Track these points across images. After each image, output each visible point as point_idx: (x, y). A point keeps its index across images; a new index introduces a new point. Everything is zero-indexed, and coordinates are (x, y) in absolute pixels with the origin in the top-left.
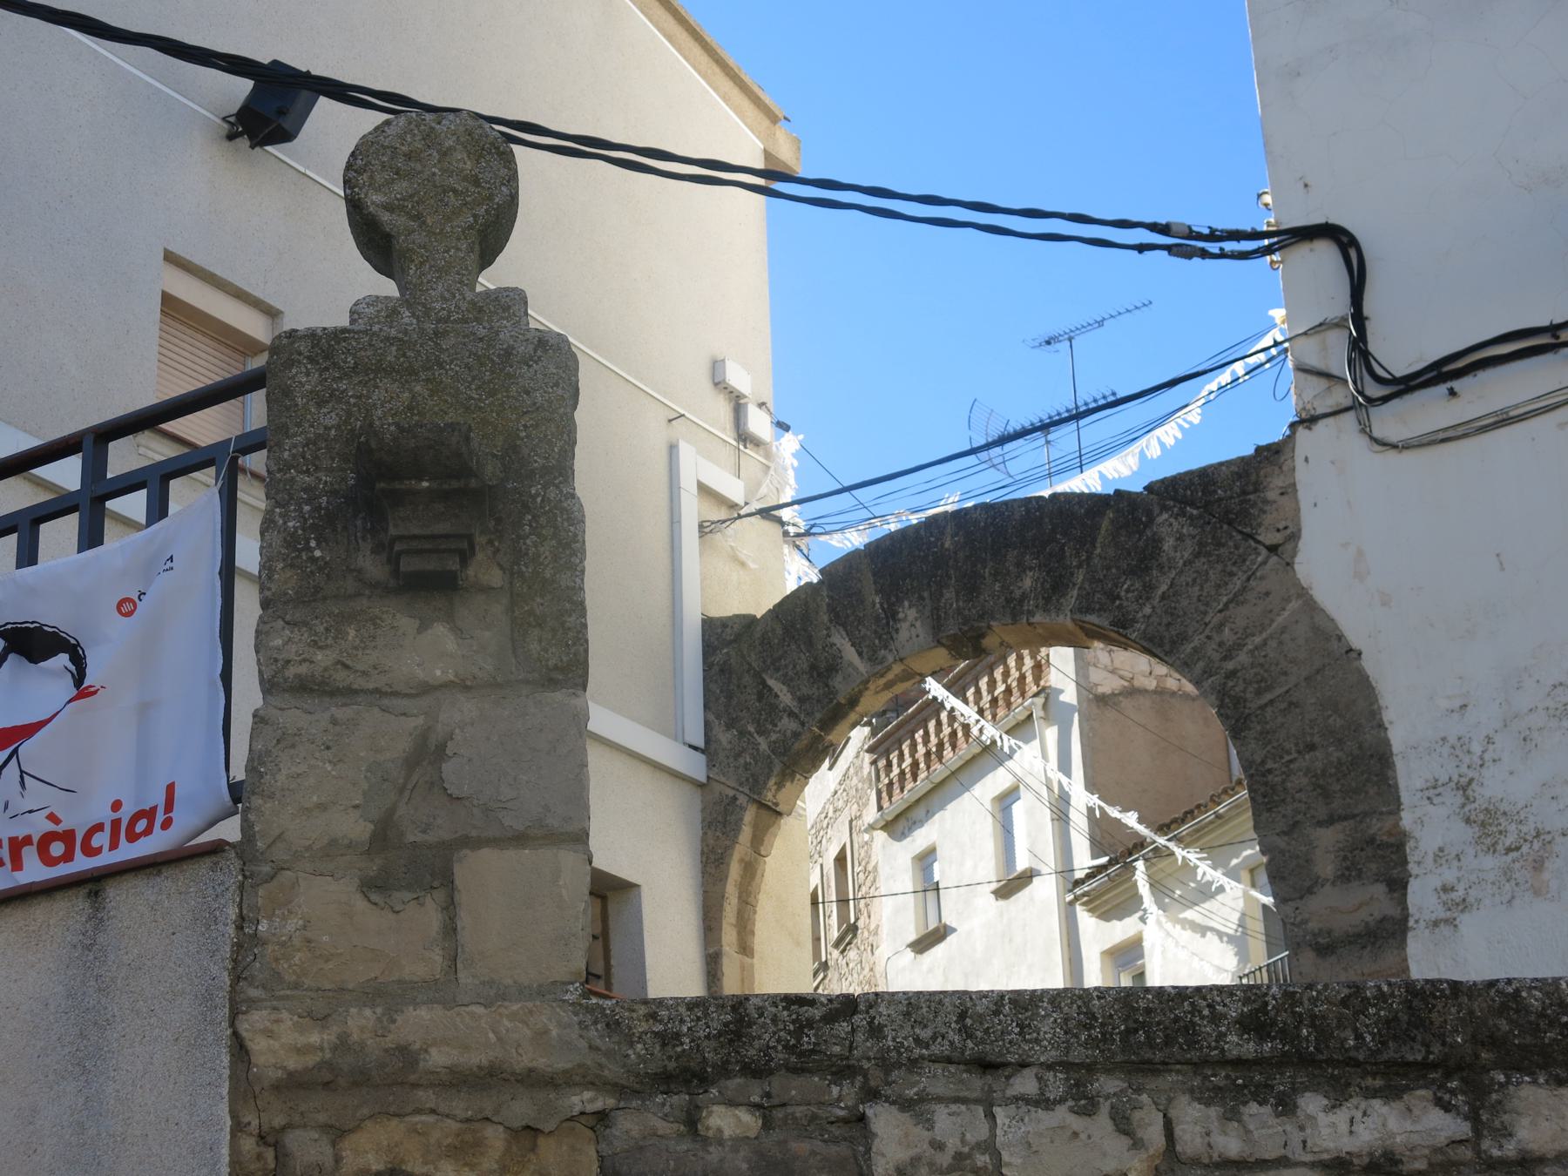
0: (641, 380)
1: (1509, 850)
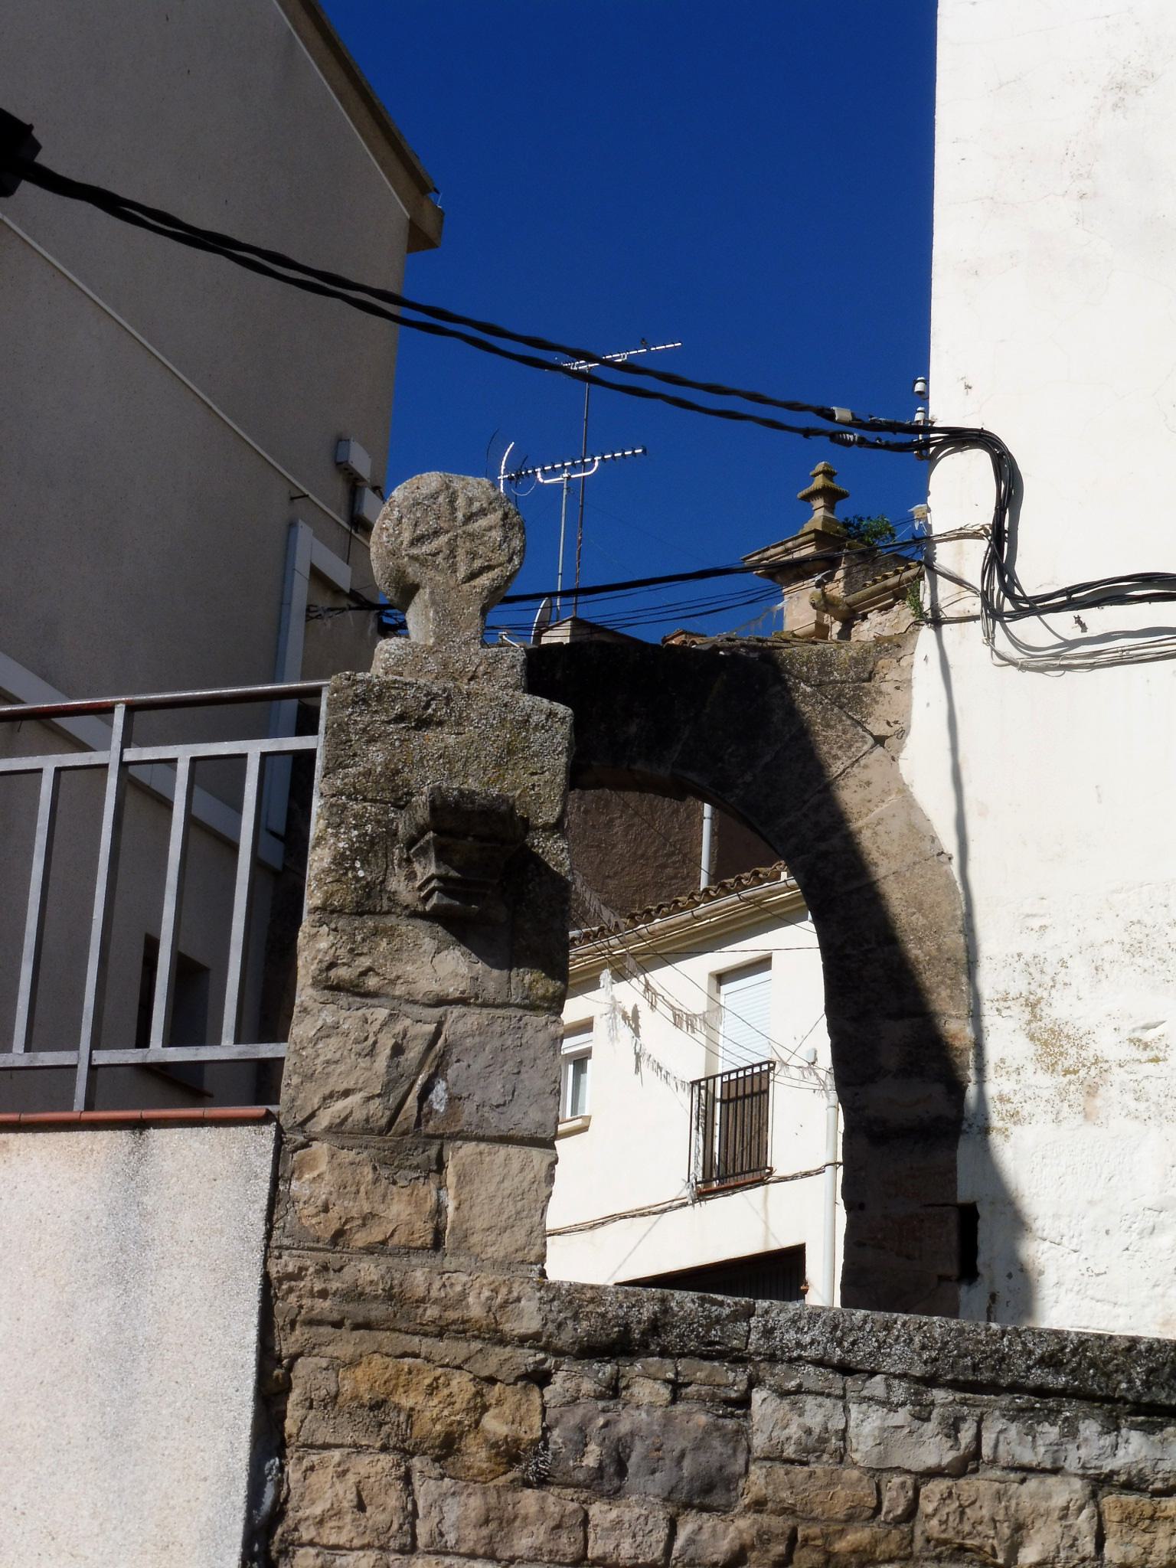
1: (1067, 1072)
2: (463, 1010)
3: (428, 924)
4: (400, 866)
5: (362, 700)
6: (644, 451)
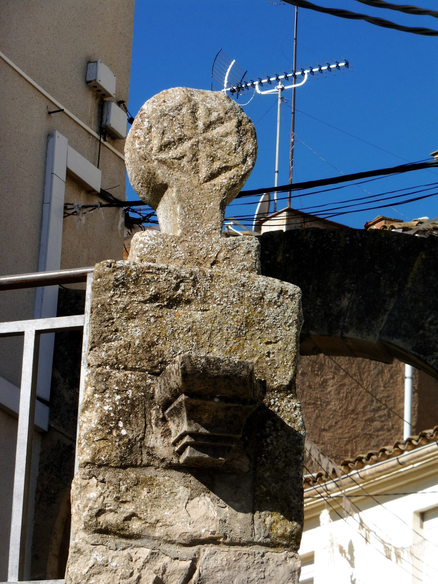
0: (31, 75)
2: (214, 548)
3: (182, 474)
4: (156, 425)
5: (121, 284)
6: (347, 64)
